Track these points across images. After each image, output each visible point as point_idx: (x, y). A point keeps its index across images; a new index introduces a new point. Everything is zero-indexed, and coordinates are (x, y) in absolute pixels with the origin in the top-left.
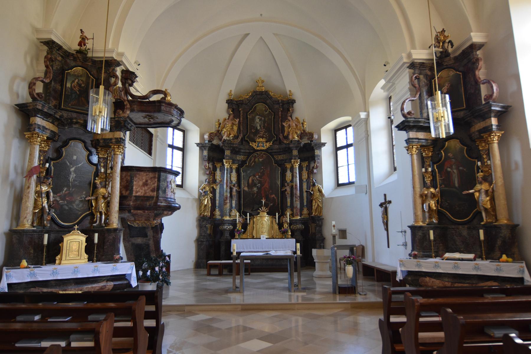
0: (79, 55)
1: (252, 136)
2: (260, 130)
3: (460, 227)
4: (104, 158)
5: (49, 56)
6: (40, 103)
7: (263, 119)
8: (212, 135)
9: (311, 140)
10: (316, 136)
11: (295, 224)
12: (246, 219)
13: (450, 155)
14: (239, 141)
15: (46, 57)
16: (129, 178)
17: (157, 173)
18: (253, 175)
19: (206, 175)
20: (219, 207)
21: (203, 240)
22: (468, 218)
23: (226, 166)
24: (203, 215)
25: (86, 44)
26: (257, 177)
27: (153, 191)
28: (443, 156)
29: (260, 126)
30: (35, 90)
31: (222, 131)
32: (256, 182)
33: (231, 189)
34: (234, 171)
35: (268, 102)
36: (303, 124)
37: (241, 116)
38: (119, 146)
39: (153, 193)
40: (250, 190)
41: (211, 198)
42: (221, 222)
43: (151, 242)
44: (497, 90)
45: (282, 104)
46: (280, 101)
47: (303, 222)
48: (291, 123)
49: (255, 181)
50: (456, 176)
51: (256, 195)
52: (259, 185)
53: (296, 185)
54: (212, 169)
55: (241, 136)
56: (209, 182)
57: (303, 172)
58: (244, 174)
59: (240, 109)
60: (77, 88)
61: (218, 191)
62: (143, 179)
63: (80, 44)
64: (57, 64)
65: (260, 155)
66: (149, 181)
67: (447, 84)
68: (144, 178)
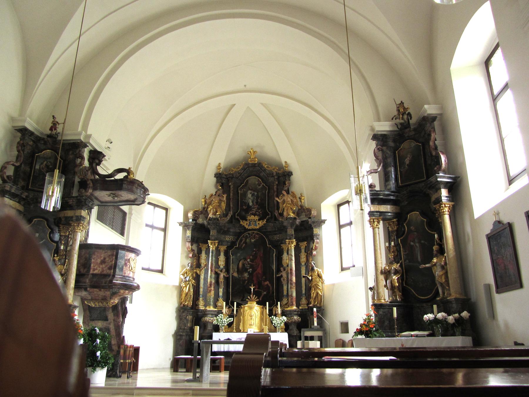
0: (49, 139)
1: (243, 213)
2: (253, 206)
3: (424, 305)
4: (65, 236)
5: (22, 142)
6: (8, 185)
7: (256, 193)
8: (197, 213)
9: (309, 216)
10: (314, 213)
11: (290, 315)
12: (233, 310)
13: (412, 228)
14: (228, 220)
15: (18, 143)
16: (88, 256)
17: (115, 251)
18: (244, 258)
19: (189, 258)
20: (203, 296)
21: (182, 334)
22: (431, 295)
23: (212, 248)
24: (184, 304)
25: (57, 129)
26: (249, 260)
27: (110, 268)
28: (406, 230)
29: (253, 202)
30: (5, 173)
31: (208, 208)
32: (247, 266)
33: (217, 275)
34: (222, 254)
35: (262, 174)
36: (300, 198)
37: (231, 191)
38: (79, 224)
39: (110, 271)
40: (240, 276)
41: (193, 285)
42: (204, 313)
43: (112, 327)
44: (445, 161)
45: (277, 177)
46: (275, 174)
47: (299, 313)
48: (285, 198)
49: (246, 266)
50: (419, 251)
51: (246, 282)
52: (251, 269)
53: (291, 270)
54: (196, 252)
55: (230, 213)
56: (191, 267)
57: (301, 254)
58: (233, 257)
59: (230, 184)
60: (45, 170)
61: (202, 277)
62: (101, 257)
63: (51, 129)
64: (28, 148)
65: (252, 235)
66: (107, 259)
67: (409, 155)
68: (102, 255)
